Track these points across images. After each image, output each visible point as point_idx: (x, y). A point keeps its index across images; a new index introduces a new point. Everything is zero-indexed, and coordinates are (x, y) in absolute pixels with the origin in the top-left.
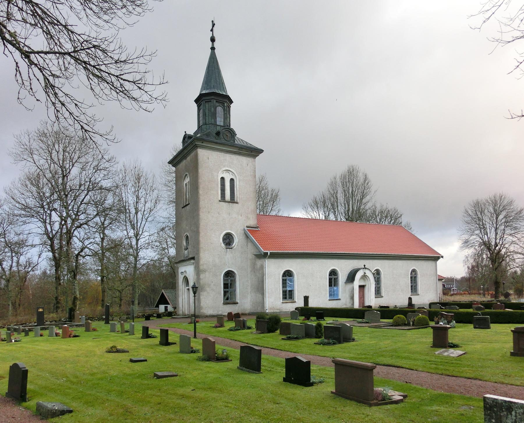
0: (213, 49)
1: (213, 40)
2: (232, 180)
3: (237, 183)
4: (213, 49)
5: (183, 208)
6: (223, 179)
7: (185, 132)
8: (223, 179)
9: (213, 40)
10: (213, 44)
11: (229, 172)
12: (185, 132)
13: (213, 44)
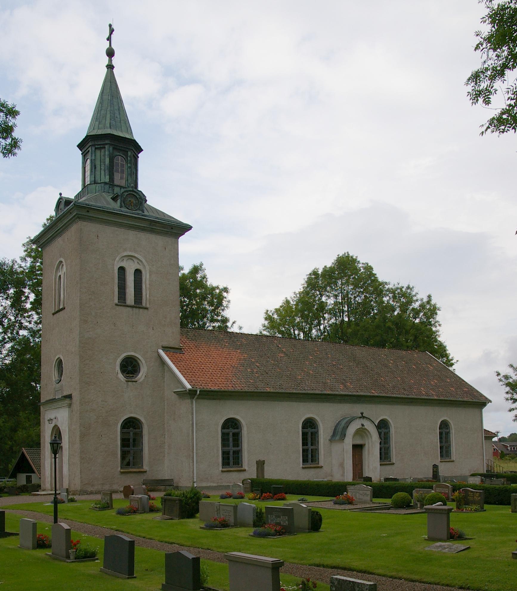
0: (110, 67)
1: (110, 53)
2: (138, 273)
3: (146, 277)
4: (110, 67)
5: (54, 314)
6: (122, 270)
7: (61, 194)
8: (122, 270)
9: (110, 53)
10: (110, 61)
11: (134, 259)
12: (61, 194)
13: (110, 61)
